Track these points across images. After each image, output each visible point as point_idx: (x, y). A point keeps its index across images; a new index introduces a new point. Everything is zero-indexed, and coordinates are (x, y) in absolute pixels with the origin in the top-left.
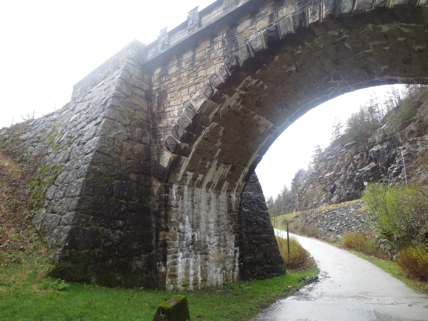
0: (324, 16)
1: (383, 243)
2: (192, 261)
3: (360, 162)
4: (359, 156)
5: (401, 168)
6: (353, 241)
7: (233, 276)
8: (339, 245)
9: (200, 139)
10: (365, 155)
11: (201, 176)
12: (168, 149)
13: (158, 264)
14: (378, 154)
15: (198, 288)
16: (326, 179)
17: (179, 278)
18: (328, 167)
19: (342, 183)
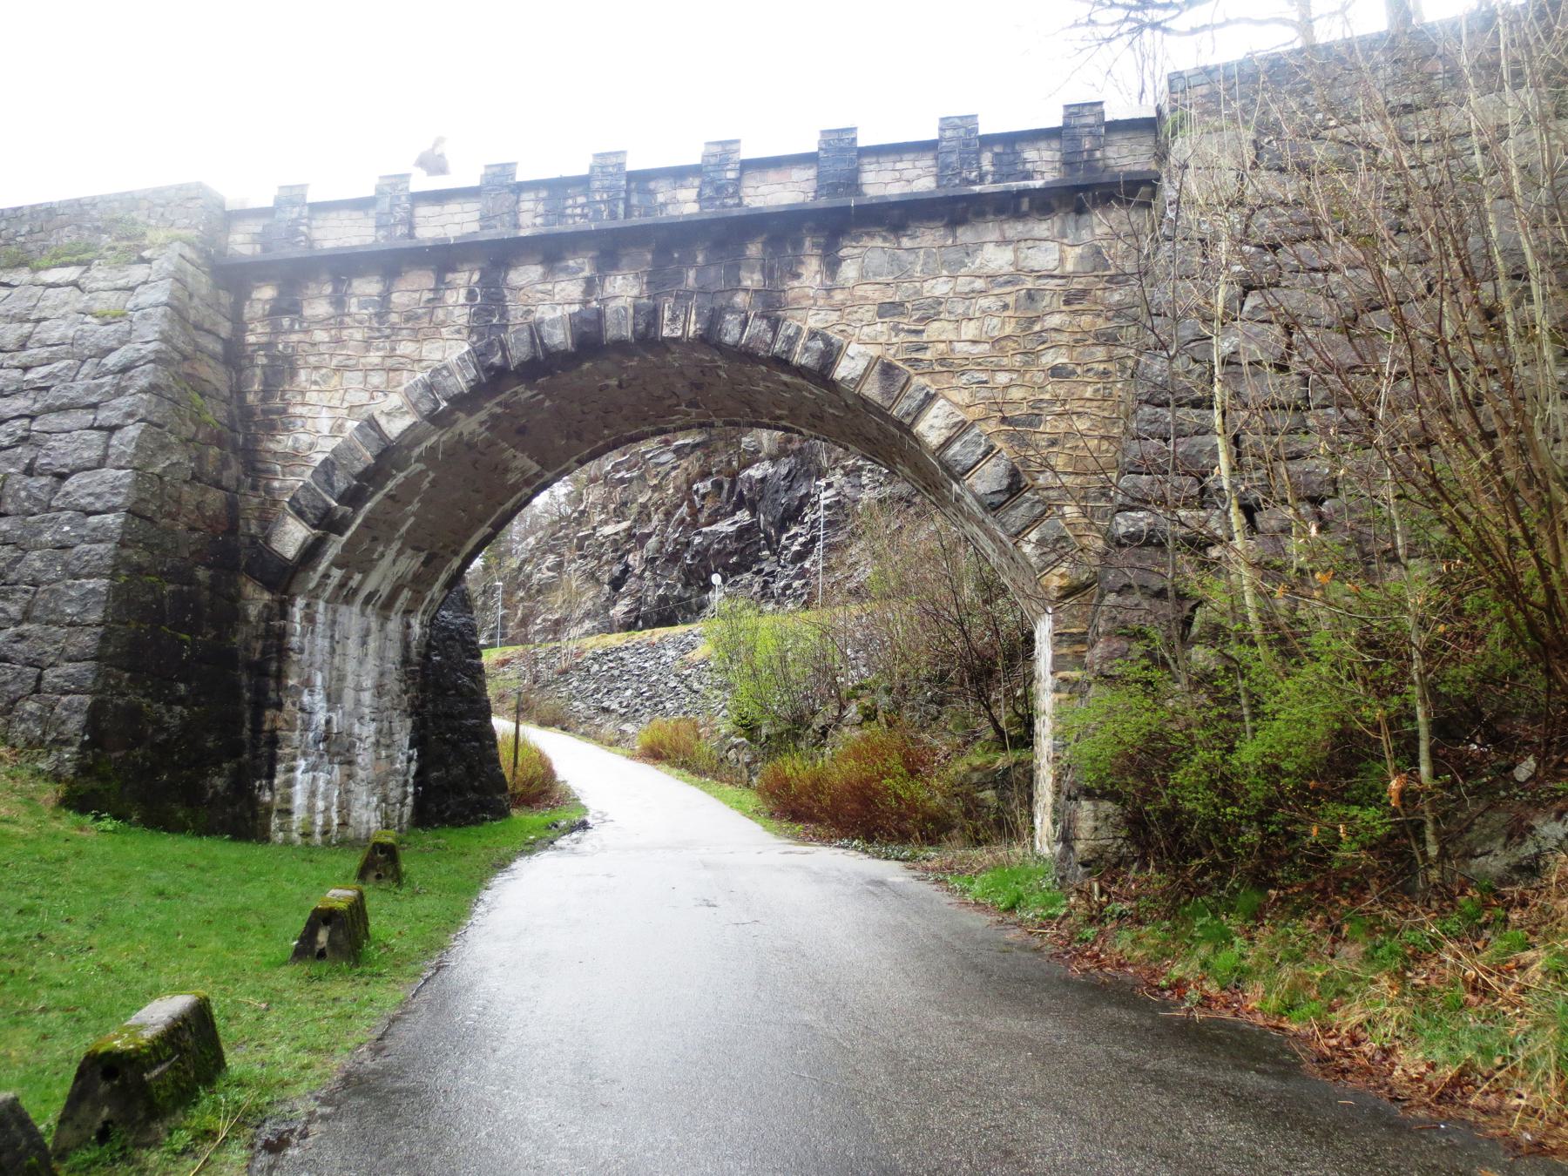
0: (691, 334)
1: (736, 746)
2: (322, 777)
3: (709, 503)
4: (709, 483)
5: (814, 540)
6: (667, 742)
7: (401, 817)
8: (627, 752)
9: (379, 497)
10: (726, 486)
11: (358, 577)
12: (300, 514)
13: (257, 784)
14: (762, 490)
15: (330, 841)
16: (603, 544)
17: (295, 817)
18: (613, 506)
19: (651, 561)
